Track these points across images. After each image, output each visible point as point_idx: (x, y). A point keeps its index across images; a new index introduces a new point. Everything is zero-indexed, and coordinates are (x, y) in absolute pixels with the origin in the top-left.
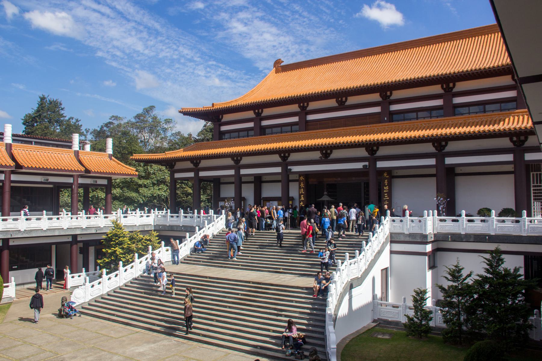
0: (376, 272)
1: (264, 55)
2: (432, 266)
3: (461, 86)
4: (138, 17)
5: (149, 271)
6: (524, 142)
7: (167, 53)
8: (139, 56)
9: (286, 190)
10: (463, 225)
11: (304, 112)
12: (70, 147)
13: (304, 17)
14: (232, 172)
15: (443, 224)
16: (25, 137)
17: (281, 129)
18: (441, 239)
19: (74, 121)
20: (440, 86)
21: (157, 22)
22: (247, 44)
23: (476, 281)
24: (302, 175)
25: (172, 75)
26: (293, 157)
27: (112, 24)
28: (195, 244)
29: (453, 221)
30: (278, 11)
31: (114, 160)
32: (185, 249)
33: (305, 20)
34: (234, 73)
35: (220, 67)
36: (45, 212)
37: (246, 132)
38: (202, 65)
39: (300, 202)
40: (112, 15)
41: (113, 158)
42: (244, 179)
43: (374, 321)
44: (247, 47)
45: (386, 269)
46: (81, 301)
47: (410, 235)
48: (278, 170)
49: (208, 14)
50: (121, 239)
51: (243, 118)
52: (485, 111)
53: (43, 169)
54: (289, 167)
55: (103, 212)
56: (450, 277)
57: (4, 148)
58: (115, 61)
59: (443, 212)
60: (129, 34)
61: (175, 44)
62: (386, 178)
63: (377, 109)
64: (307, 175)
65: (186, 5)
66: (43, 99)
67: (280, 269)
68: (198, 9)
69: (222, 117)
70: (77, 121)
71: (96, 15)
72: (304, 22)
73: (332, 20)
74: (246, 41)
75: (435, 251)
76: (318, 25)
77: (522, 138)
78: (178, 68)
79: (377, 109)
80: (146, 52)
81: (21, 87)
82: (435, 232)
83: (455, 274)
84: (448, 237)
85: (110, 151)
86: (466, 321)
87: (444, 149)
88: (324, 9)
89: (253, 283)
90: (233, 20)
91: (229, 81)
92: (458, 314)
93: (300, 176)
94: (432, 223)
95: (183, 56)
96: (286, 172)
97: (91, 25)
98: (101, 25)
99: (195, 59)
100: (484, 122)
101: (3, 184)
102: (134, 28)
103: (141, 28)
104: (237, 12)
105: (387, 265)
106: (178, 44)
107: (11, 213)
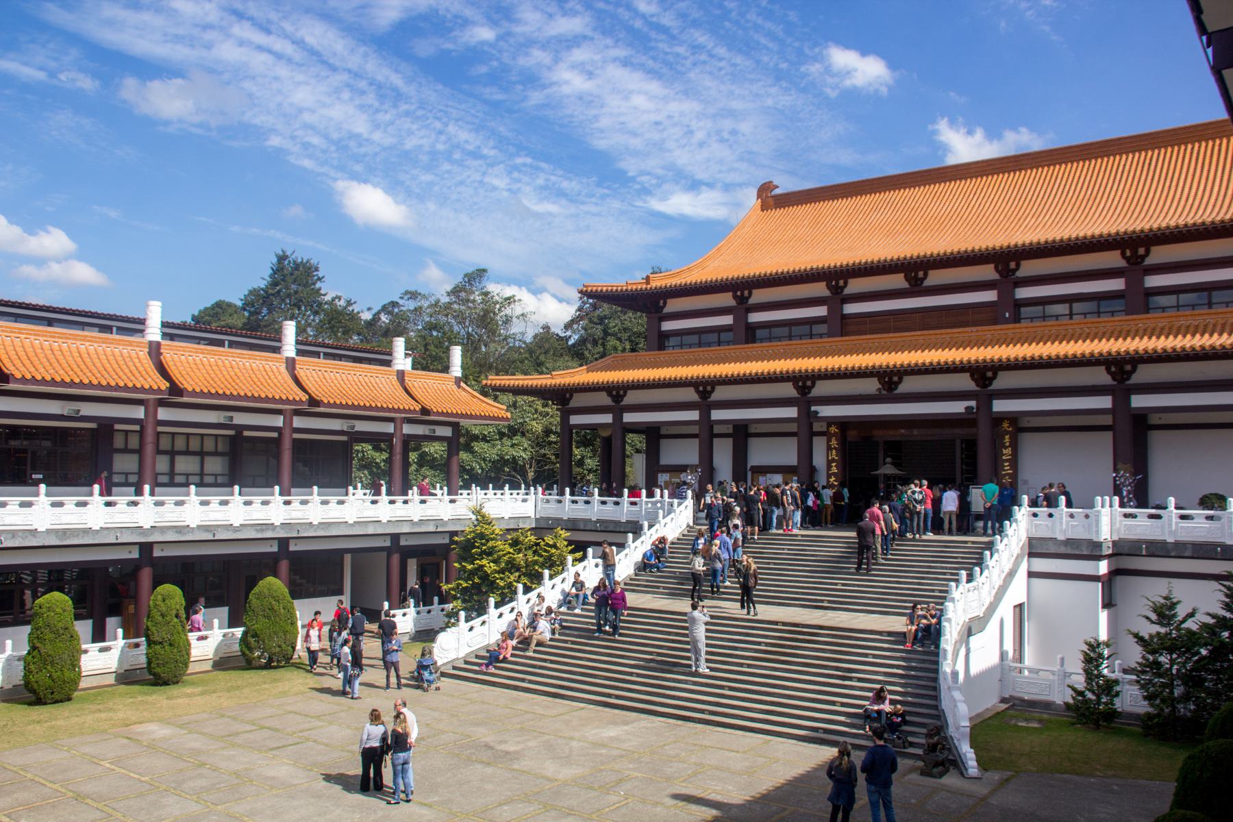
0: (1005, 611)
1: (636, 143)
2: (1108, 604)
3: (1160, 254)
4: (354, 61)
5: (570, 602)
6: (897, 384)
7: (422, 137)
8: (360, 145)
9: (806, 453)
10: (1170, 525)
12: (277, 350)
13: (721, 59)
14: (694, 415)
15: (1130, 522)
16: (196, 330)
18: (1126, 551)
19: (342, 303)
20: (1119, 252)
21: (396, 71)
22: (596, 118)
23: (1205, 626)
24: (835, 424)
25: (436, 189)
27: (300, 77)
28: (645, 555)
30: (660, 45)
31: (464, 390)
32: (626, 564)
33: (722, 64)
34: (574, 183)
35: (542, 170)
36: (315, 488)
38: (501, 166)
39: (829, 476)
40: (298, 56)
41: (462, 384)
42: (717, 429)
43: (1003, 700)
44: (596, 125)
45: (1021, 606)
46: (452, 656)
47: (1069, 542)
48: (792, 412)
49: (506, 54)
50: (490, 544)
52: (1210, 305)
53: (353, 407)
54: (813, 408)
56: (1154, 617)
57: (284, 365)
58: (310, 157)
59: (1130, 500)
60: (338, 98)
61: (439, 119)
62: (1007, 433)
63: (990, 296)
64: (844, 425)
65: (455, 33)
66: (282, 258)
67: (822, 601)
68: (483, 43)
69: (665, 303)
70: (349, 303)
71: (264, 57)
72: (721, 69)
73: (784, 66)
74: (594, 112)
75: (1115, 573)
76: (752, 76)
77: (1128, 367)
78: (449, 172)
79: (990, 296)
80: (377, 136)
81: (113, 214)
82: (1115, 538)
83: (1164, 613)
84: (1141, 548)
85: (456, 370)
86: (1186, 698)
88: (763, 41)
89: (784, 624)
90: (562, 65)
91: (564, 202)
92: (1171, 686)
93: (829, 425)
94: (1109, 521)
95: (458, 146)
96: (807, 417)
97: (254, 78)
98: (276, 79)
99: (485, 151)
100: (1211, 327)
101: (280, 434)
102: (348, 85)
103: (362, 84)
104: (569, 48)
105: (1023, 599)
106: (445, 120)
107: (293, 490)
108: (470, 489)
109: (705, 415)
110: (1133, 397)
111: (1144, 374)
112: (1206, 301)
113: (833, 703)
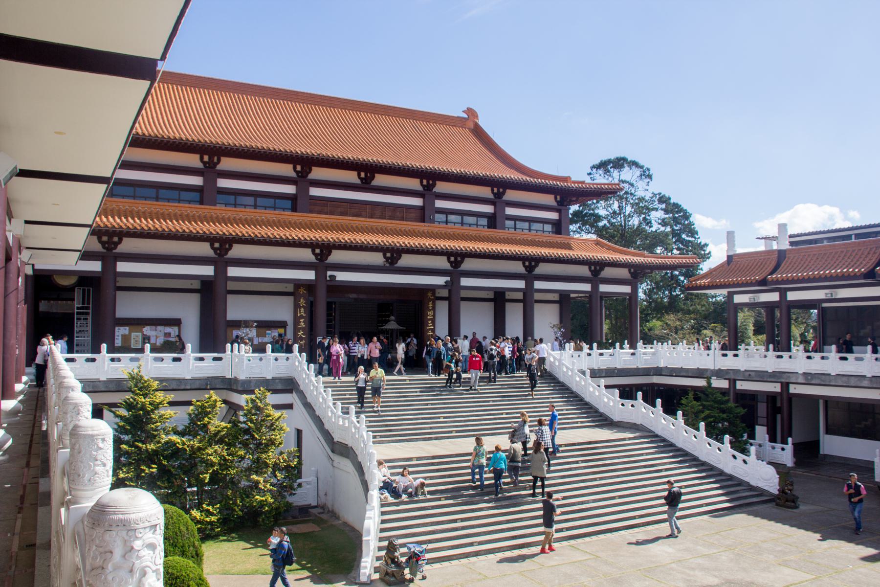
6: (116, 244)
11: (302, 180)
14: (521, 284)
17: (157, 193)
26: (337, 256)
29: (215, 359)
37: (155, 190)
51: (176, 164)
55: (838, 347)
77: (116, 239)
87: (115, 248)
108: (652, 344)
109: (530, 285)
110: (119, 264)
111: (238, 251)
112: (198, 199)
113: (613, 498)
